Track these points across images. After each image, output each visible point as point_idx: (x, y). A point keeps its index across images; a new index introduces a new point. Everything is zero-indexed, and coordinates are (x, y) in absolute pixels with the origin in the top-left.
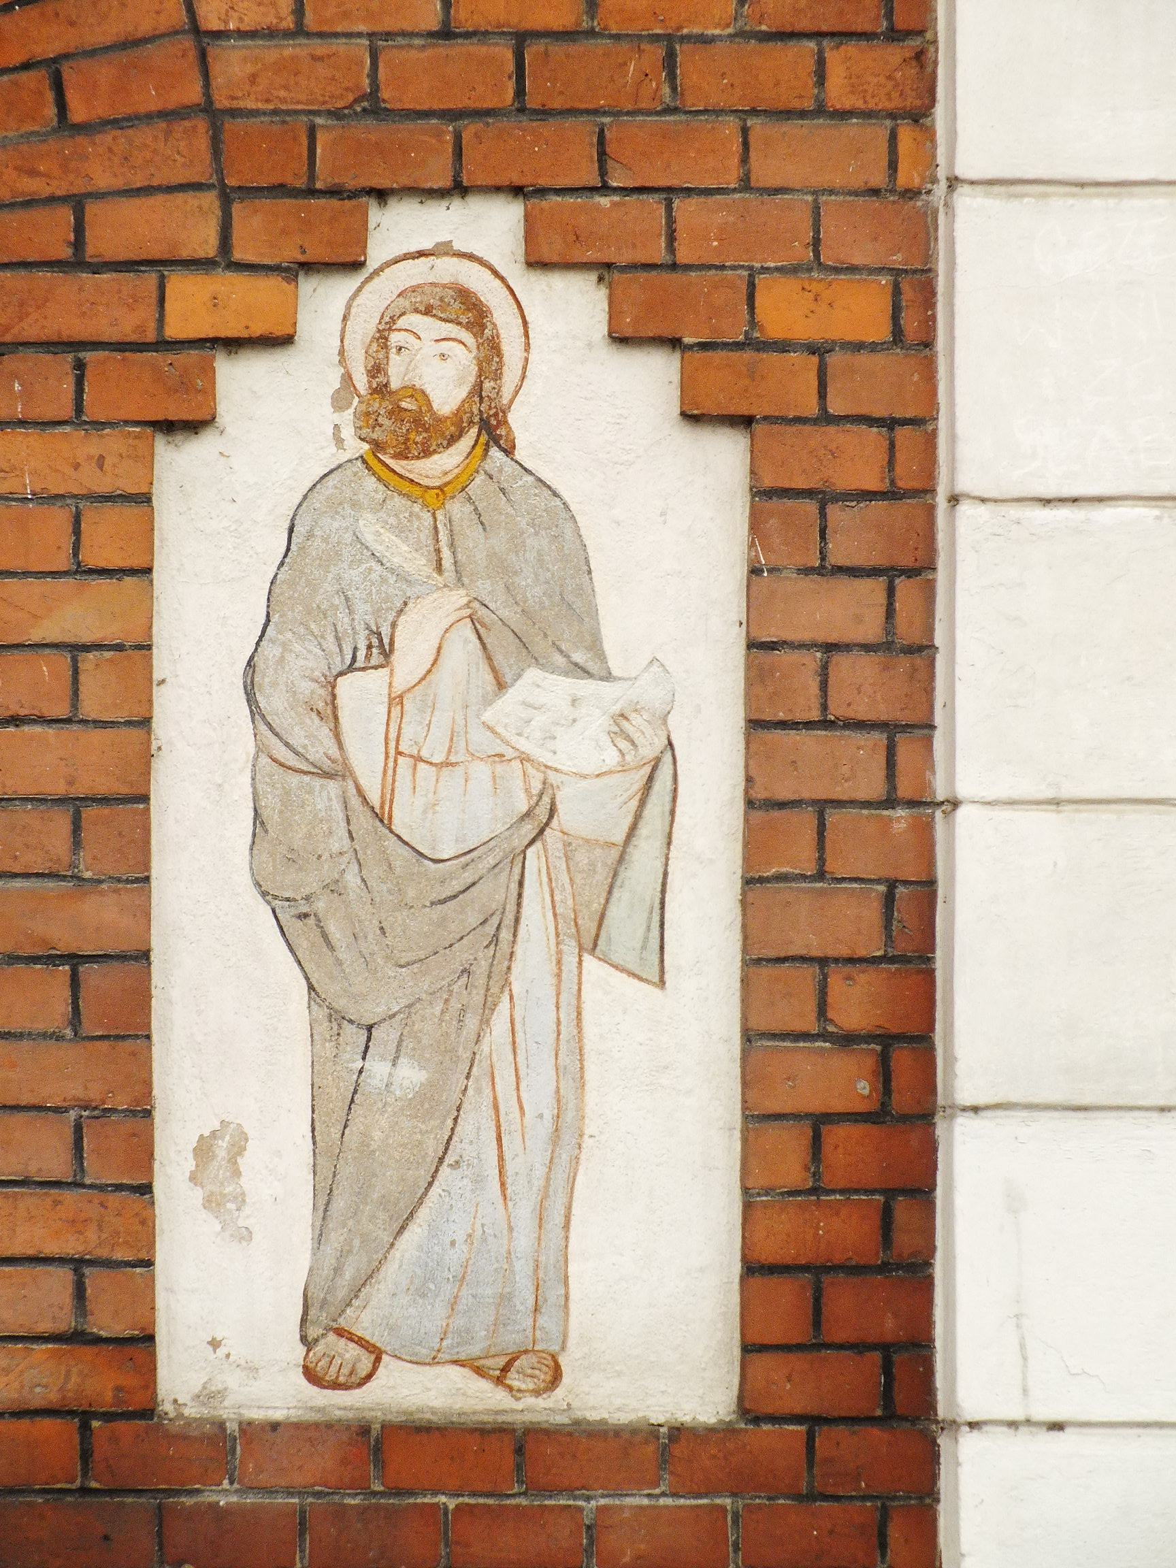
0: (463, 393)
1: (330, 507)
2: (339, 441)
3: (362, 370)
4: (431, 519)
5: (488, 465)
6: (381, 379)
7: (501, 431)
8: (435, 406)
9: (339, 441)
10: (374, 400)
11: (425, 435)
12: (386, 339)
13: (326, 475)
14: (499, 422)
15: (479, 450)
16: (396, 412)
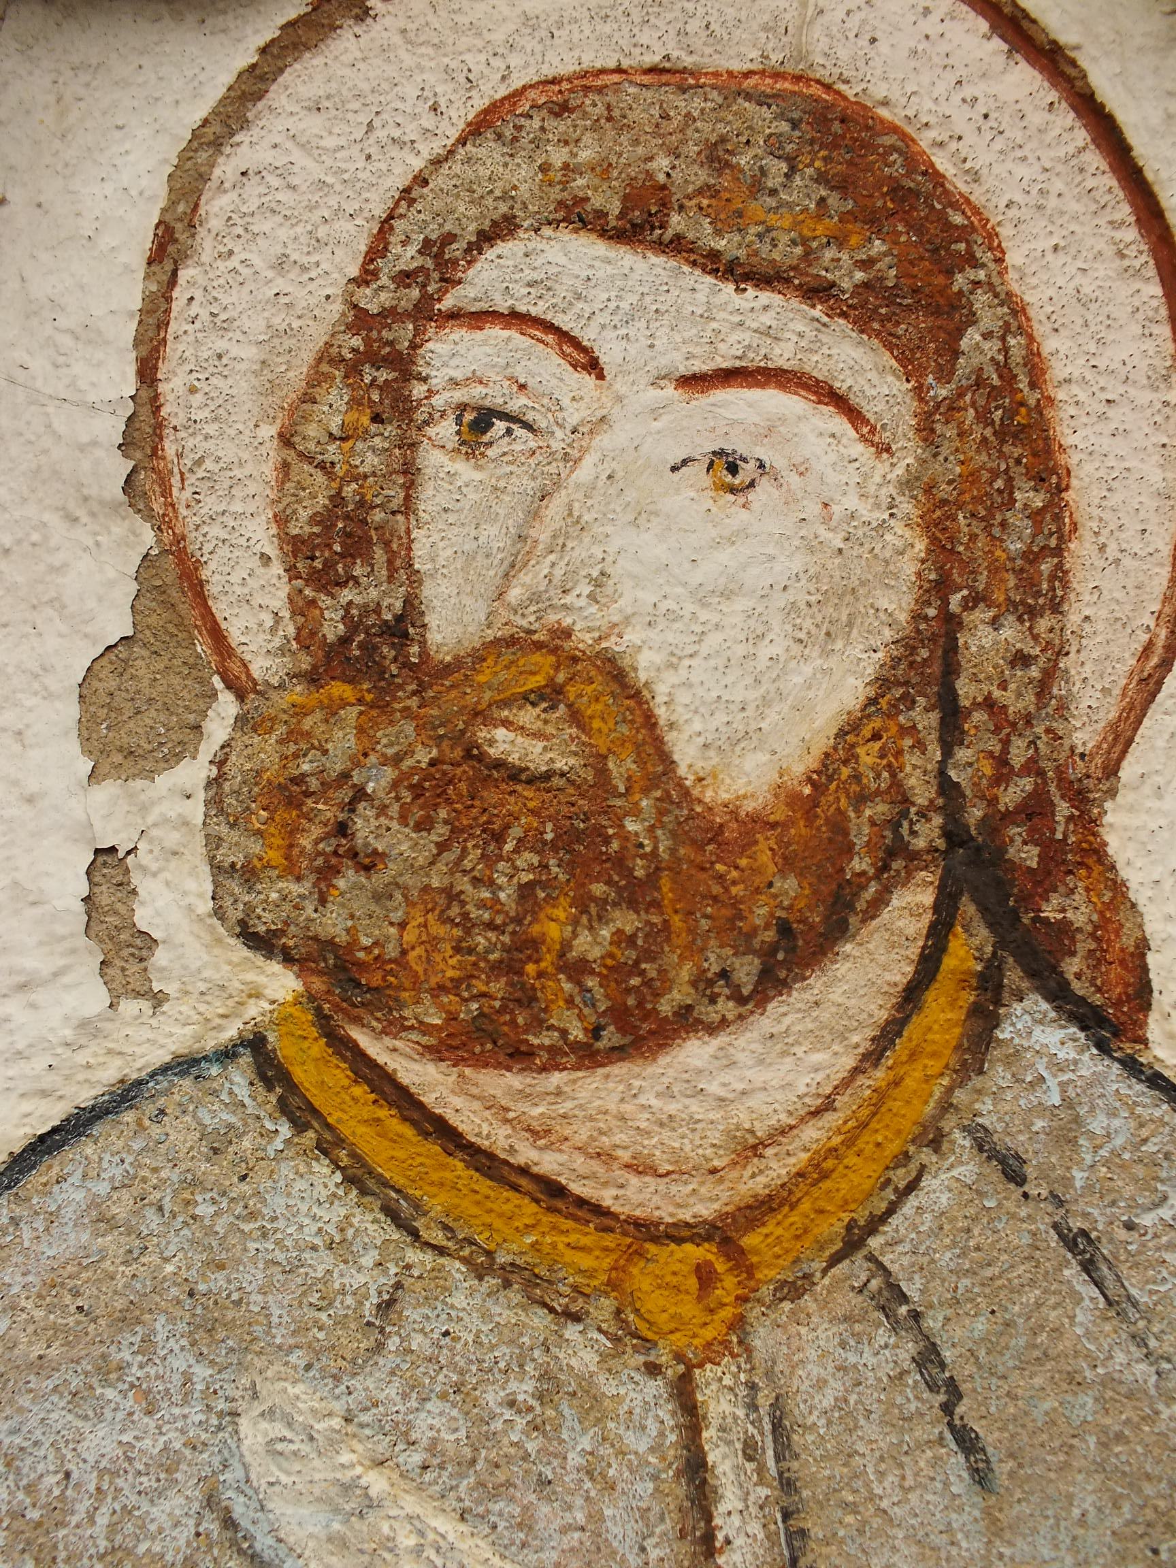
0: (840, 683)
1: (70, 1338)
2: (123, 951)
3: (261, 534)
4: (666, 1412)
5: (997, 1102)
6: (371, 591)
7: (1071, 907)
8: (687, 755)
9: (123, 951)
10: (332, 710)
11: (626, 921)
12: (404, 365)
13: (45, 1145)
14: (1052, 853)
15: (942, 1015)
16: (460, 787)
